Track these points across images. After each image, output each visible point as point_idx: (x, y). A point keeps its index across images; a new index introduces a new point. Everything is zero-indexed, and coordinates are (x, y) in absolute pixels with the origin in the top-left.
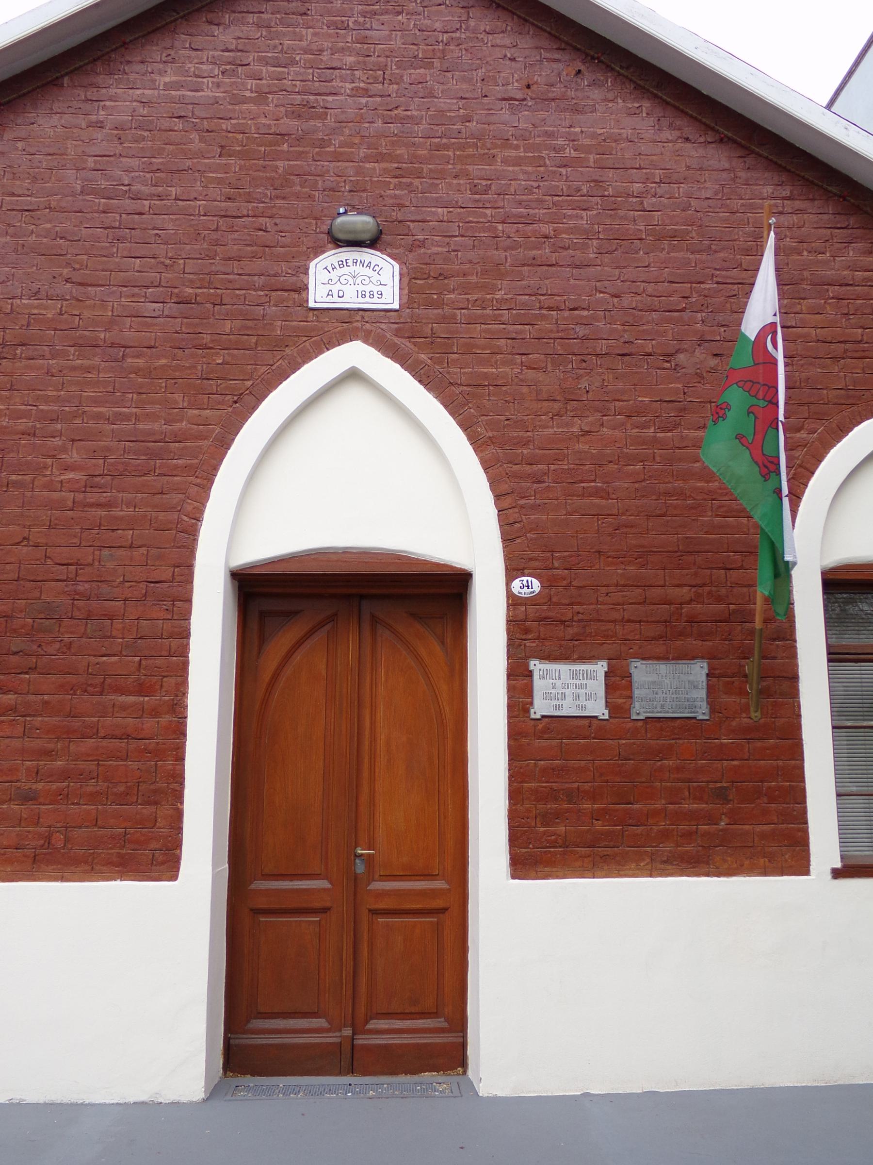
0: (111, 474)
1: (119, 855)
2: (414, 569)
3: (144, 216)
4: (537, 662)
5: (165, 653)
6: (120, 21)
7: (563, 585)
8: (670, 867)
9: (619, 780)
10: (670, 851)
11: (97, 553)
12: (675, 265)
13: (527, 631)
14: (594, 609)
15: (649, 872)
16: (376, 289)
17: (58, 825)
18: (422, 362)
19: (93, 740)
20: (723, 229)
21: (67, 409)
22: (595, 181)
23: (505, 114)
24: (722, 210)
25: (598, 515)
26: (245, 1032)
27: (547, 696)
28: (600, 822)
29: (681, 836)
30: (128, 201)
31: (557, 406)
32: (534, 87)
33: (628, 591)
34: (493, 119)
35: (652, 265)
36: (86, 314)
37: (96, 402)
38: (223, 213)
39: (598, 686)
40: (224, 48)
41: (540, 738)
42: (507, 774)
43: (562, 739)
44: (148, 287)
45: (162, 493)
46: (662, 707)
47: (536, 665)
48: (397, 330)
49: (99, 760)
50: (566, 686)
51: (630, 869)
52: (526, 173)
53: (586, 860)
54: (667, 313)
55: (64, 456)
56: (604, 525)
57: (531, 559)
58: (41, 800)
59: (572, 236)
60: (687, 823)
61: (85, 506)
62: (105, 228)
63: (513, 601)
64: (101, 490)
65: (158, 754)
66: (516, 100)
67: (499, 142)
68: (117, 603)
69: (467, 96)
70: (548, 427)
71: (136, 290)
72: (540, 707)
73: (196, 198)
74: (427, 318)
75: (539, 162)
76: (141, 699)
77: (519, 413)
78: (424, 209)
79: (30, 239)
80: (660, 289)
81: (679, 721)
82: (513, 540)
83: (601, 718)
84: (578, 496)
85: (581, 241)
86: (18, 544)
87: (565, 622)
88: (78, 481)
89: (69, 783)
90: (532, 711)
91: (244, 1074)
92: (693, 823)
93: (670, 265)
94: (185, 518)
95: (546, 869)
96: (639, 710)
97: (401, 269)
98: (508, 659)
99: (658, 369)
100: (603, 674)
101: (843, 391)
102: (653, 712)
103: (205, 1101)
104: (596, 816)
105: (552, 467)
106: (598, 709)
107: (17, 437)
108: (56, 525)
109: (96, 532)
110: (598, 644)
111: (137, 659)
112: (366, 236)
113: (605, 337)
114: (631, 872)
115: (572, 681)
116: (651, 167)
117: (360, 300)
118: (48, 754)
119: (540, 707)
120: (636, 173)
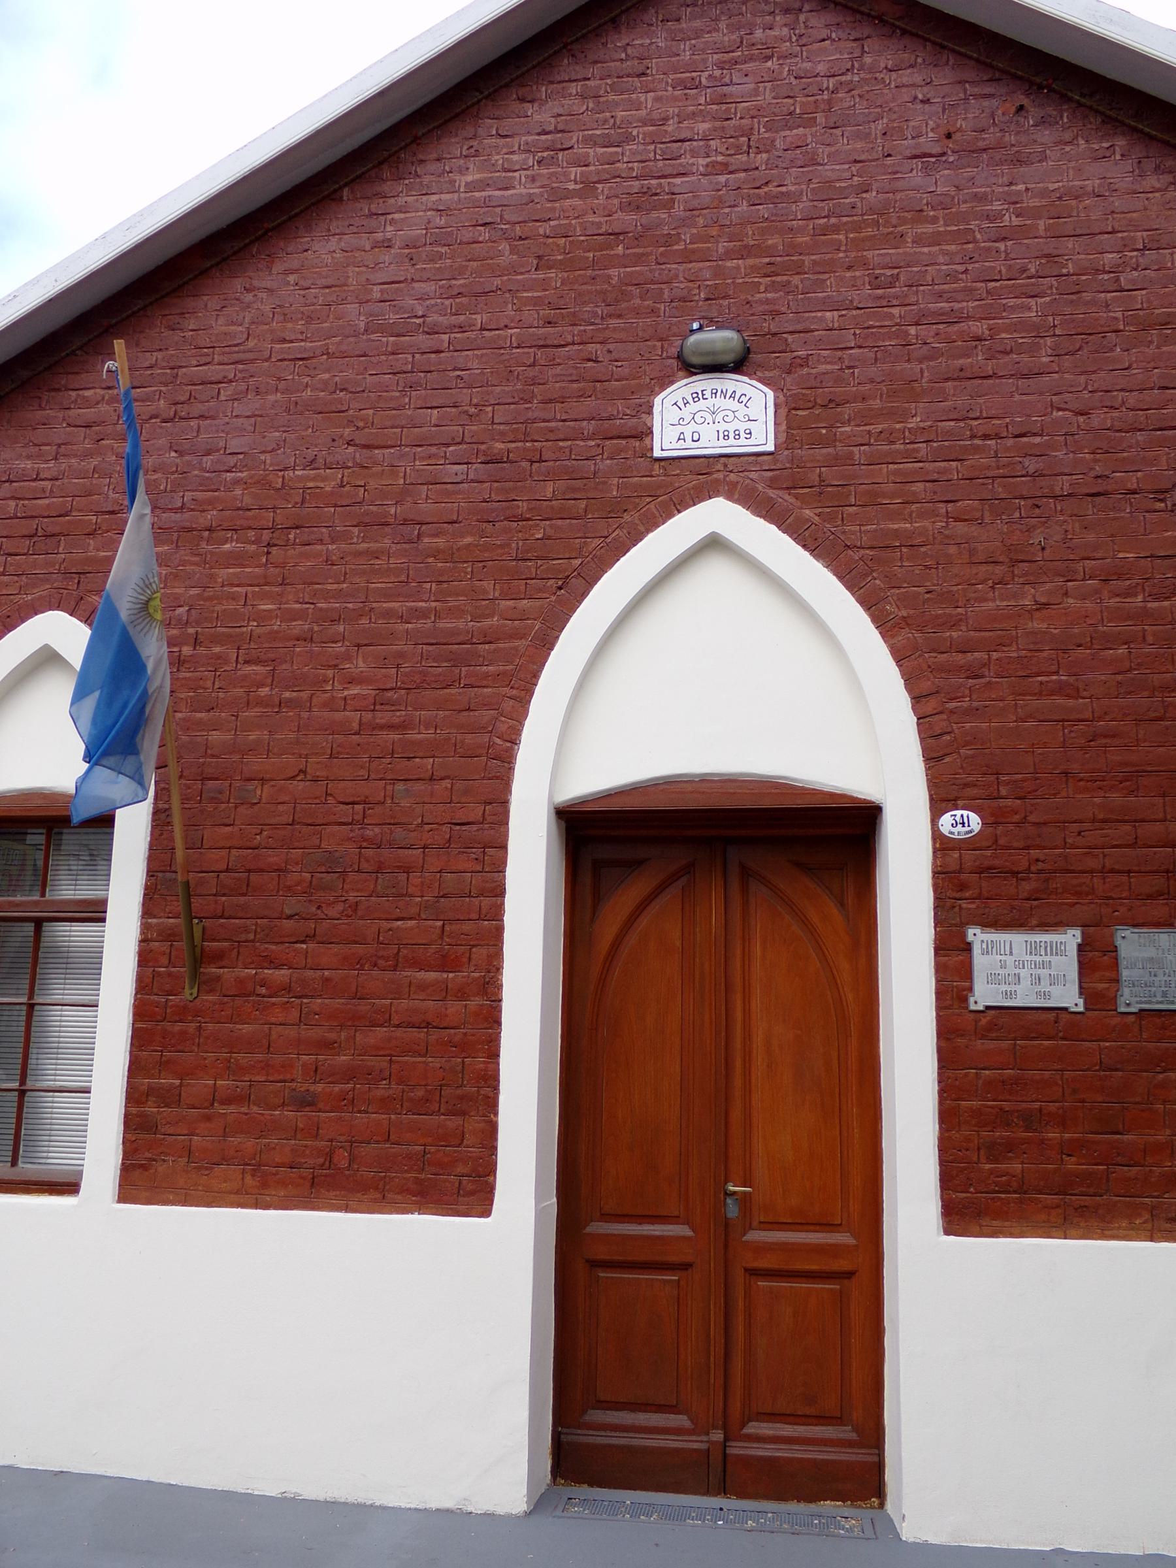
0: (406, 686)
1: (417, 1181)
3: (442, 355)
4: (978, 931)
5: (475, 916)
7: (1014, 820)
11: (389, 787)
13: (962, 887)
14: (1060, 855)
16: (742, 427)
17: (342, 1138)
18: (808, 520)
19: (385, 1029)
21: (350, 606)
23: (916, 177)
25: (1063, 721)
27: (993, 979)
28: (1073, 1159)
30: (422, 337)
31: (999, 570)
32: (955, 137)
34: (900, 185)
35: (1135, 366)
36: (373, 484)
37: (388, 596)
38: (541, 343)
39: (1068, 964)
41: (983, 1037)
42: (936, 1088)
43: (1015, 1039)
44: (448, 445)
45: (469, 709)
47: (976, 936)
48: (772, 479)
49: (391, 1055)
50: (1021, 964)
51: (1119, 1228)
55: (347, 666)
56: (1073, 735)
57: (966, 785)
58: (321, 1105)
59: (1015, 335)
61: (374, 729)
62: (394, 374)
63: (942, 845)
64: (393, 708)
65: (465, 1047)
66: (931, 156)
67: (908, 215)
68: (414, 852)
69: (863, 158)
70: (986, 600)
71: (433, 450)
72: (984, 995)
73: (506, 326)
75: (966, 237)
76: (445, 975)
77: (945, 582)
79: (304, 394)
83: (1072, 1010)
86: (293, 778)
88: (365, 697)
89: (355, 1084)
90: (972, 1000)
93: (1161, 364)
94: (498, 741)
95: (994, 1223)
96: (1129, 1000)
97: (776, 398)
98: (935, 927)
99: (1147, 512)
103: (528, 1514)
104: (1069, 1148)
105: (995, 655)
106: (1068, 997)
107: (290, 644)
108: (338, 753)
111: (440, 923)
112: (728, 358)
115: (1028, 958)
117: (722, 442)
118: (327, 1046)
119: (984, 995)
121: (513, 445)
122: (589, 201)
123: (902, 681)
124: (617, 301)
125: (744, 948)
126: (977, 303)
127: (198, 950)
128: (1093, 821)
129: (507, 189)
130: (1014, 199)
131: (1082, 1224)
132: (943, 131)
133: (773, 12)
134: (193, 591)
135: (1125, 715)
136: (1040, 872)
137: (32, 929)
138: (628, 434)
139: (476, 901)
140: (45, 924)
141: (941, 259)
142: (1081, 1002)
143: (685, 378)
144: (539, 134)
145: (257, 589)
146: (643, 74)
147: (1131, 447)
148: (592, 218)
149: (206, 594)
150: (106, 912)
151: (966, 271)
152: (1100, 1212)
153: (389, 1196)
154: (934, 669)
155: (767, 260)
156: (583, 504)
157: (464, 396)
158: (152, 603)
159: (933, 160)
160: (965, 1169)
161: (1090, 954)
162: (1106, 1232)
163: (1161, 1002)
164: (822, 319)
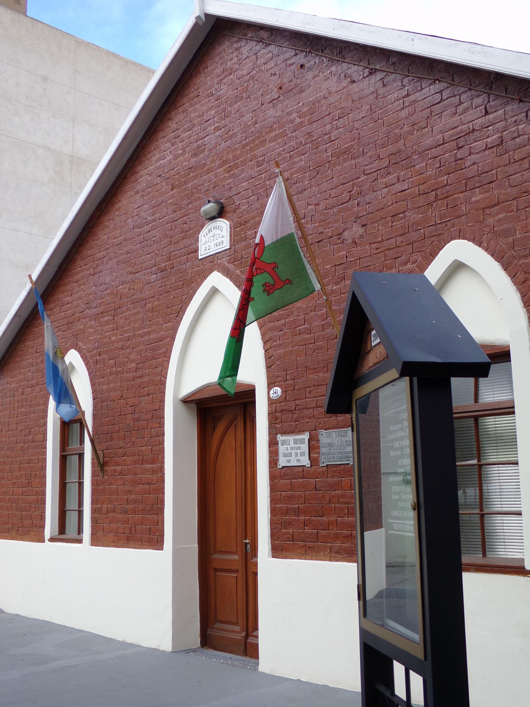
1: (149, 538)
2: (240, 389)
6: (141, 135)
7: (291, 389)
8: (339, 556)
9: (315, 503)
10: (339, 547)
12: (345, 172)
13: (276, 419)
14: (304, 402)
15: (304, 557)
20: (370, 135)
21: (131, 334)
22: (308, 133)
24: (371, 122)
25: (306, 345)
26: (212, 628)
27: (285, 455)
29: (344, 537)
30: (146, 227)
32: (283, 87)
33: (319, 389)
34: (266, 116)
37: (139, 329)
38: (173, 220)
39: (305, 447)
40: (172, 131)
42: (269, 500)
43: (291, 479)
44: (152, 268)
45: (156, 367)
46: (334, 458)
47: (280, 438)
51: (321, 556)
52: (279, 143)
53: (303, 549)
54: (341, 206)
56: (308, 350)
57: (278, 377)
60: (347, 529)
66: (275, 99)
67: (268, 130)
72: (282, 462)
74: (240, 249)
76: (153, 465)
78: (239, 186)
80: (338, 191)
81: (343, 466)
82: (270, 367)
83: (307, 466)
84: (297, 335)
85: (301, 176)
86: (120, 399)
87: (292, 411)
90: (278, 464)
91: (211, 648)
92: (349, 529)
95: (286, 553)
96: (324, 461)
98: (269, 436)
99: (335, 245)
100: (307, 440)
101: (433, 226)
102: (330, 462)
104: (305, 523)
105: (287, 320)
106: (305, 461)
109: (139, 390)
110: (306, 422)
112: (214, 214)
113: (311, 233)
114: (322, 558)
116: (335, 110)
118: (130, 492)
119: (282, 462)
120: (327, 118)
121: (166, 263)
122: (184, 156)
123: (510, 278)
124: (191, 197)
125: (251, 446)
126: (287, 163)
127: (102, 462)
128: (314, 386)
129: (164, 159)
130: (299, 110)
131: (311, 554)
132: (278, 87)
133: (233, 52)
134: (99, 336)
135: (324, 339)
136: (298, 410)
137: (473, 422)
138: (193, 251)
139: (158, 438)
140: (480, 419)
141: (277, 147)
142: (309, 462)
143: (209, 222)
144: (172, 133)
145: (111, 332)
146: (198, 95)
147: (331, 216)
148: (185, 164)
149: (102, 337)
150: (514, 407)
151: (284, 150)
152: (316, 549)
153: (143, 543)
154: (272, 329)
155: (228, 165)
156: (182, 282)
157: (155, 247)
158: (57, 352)
159: (276, 101)
160: (278, 532)
161: (313, 442)
162: (318, 557)
163: (332, 461)
164: (243, 186)
